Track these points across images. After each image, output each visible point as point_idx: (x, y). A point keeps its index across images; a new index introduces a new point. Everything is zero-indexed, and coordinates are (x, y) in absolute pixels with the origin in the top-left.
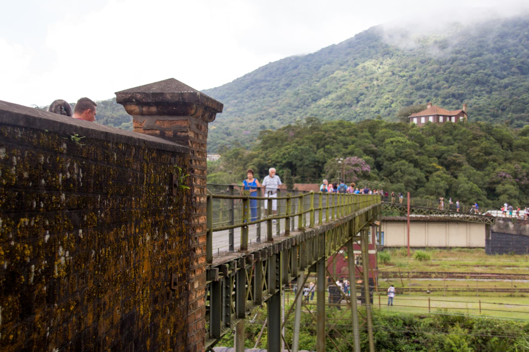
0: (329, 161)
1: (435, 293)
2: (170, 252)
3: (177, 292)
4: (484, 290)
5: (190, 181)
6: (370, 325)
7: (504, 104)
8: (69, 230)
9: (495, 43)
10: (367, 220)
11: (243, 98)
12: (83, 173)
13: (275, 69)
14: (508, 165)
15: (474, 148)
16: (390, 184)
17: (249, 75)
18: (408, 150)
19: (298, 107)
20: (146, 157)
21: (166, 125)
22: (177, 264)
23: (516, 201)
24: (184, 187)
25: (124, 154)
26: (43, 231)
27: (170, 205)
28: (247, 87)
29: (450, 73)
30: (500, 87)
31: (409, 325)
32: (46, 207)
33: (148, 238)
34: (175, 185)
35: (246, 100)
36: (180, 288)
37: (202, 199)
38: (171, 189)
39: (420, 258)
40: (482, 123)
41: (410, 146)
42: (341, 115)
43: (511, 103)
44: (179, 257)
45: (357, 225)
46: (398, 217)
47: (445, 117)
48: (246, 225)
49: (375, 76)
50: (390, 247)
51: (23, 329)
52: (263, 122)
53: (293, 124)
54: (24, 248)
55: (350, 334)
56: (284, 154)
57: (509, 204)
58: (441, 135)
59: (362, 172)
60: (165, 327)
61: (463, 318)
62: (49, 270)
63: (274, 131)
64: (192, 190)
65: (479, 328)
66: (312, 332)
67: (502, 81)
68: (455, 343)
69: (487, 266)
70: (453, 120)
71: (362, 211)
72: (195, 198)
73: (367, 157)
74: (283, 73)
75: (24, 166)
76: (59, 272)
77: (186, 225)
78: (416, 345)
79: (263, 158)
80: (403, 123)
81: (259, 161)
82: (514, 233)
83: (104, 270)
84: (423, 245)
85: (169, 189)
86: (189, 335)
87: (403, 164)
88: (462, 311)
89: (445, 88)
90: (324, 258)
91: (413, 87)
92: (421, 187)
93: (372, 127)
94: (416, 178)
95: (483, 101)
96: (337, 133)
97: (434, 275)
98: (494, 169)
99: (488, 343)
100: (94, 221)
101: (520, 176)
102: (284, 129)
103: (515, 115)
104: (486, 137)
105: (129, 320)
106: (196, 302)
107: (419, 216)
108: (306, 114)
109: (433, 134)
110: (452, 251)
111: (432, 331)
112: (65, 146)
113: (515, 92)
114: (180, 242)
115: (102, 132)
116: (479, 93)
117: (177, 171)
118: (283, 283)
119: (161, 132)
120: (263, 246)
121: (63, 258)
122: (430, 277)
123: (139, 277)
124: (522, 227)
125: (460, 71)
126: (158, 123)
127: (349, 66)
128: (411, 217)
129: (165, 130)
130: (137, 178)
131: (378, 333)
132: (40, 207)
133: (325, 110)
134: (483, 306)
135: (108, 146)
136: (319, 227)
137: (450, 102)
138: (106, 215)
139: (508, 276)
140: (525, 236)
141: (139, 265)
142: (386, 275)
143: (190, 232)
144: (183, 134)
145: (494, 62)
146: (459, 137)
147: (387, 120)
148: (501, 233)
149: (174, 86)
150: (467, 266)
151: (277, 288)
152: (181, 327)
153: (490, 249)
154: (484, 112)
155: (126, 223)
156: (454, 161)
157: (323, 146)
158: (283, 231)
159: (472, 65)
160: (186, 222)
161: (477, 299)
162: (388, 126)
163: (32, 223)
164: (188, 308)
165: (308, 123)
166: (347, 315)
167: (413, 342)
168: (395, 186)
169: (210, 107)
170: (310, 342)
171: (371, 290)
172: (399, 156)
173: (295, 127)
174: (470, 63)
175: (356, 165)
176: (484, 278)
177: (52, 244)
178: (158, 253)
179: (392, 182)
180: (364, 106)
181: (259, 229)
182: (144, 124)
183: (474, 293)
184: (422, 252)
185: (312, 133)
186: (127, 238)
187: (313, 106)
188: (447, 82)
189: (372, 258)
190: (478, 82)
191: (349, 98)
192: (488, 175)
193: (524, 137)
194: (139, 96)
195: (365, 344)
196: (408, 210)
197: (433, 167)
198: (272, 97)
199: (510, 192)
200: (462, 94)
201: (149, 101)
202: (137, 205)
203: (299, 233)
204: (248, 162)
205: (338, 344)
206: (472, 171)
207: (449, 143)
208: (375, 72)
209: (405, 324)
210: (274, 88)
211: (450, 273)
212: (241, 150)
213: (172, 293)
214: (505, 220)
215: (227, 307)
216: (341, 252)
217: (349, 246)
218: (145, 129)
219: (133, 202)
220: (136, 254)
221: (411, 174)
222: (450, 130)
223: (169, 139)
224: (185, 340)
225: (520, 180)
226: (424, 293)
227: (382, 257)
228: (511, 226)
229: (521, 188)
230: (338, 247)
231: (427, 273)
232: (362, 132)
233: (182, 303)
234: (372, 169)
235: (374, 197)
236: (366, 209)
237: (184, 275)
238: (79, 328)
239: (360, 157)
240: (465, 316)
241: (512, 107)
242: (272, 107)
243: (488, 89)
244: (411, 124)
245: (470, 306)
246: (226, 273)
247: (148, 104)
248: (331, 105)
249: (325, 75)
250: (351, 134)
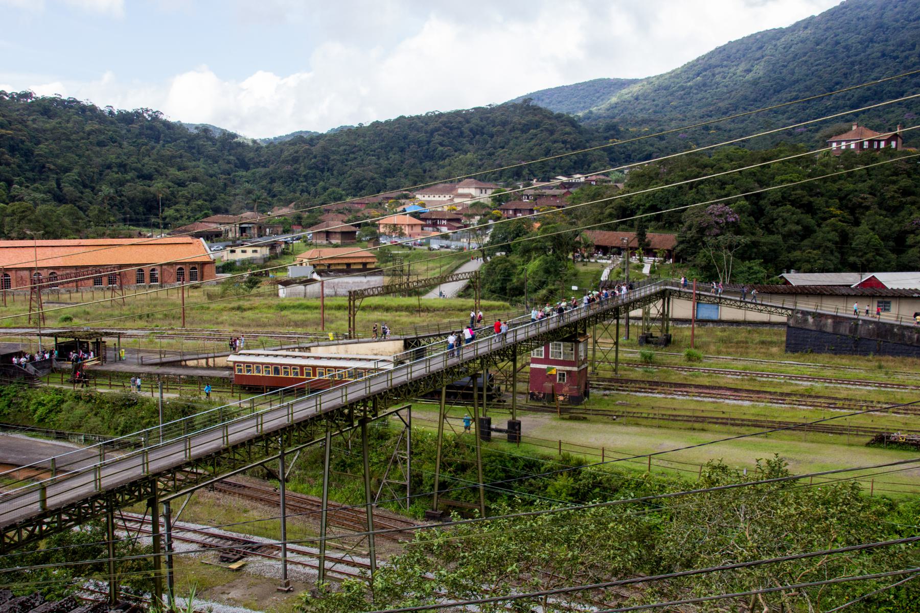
13: (734, 51)
82: (814, 328)
98: (911, 214)
140: (825, 332)
148: (798, 328)
180: (837, 99)
228: (810, 320)
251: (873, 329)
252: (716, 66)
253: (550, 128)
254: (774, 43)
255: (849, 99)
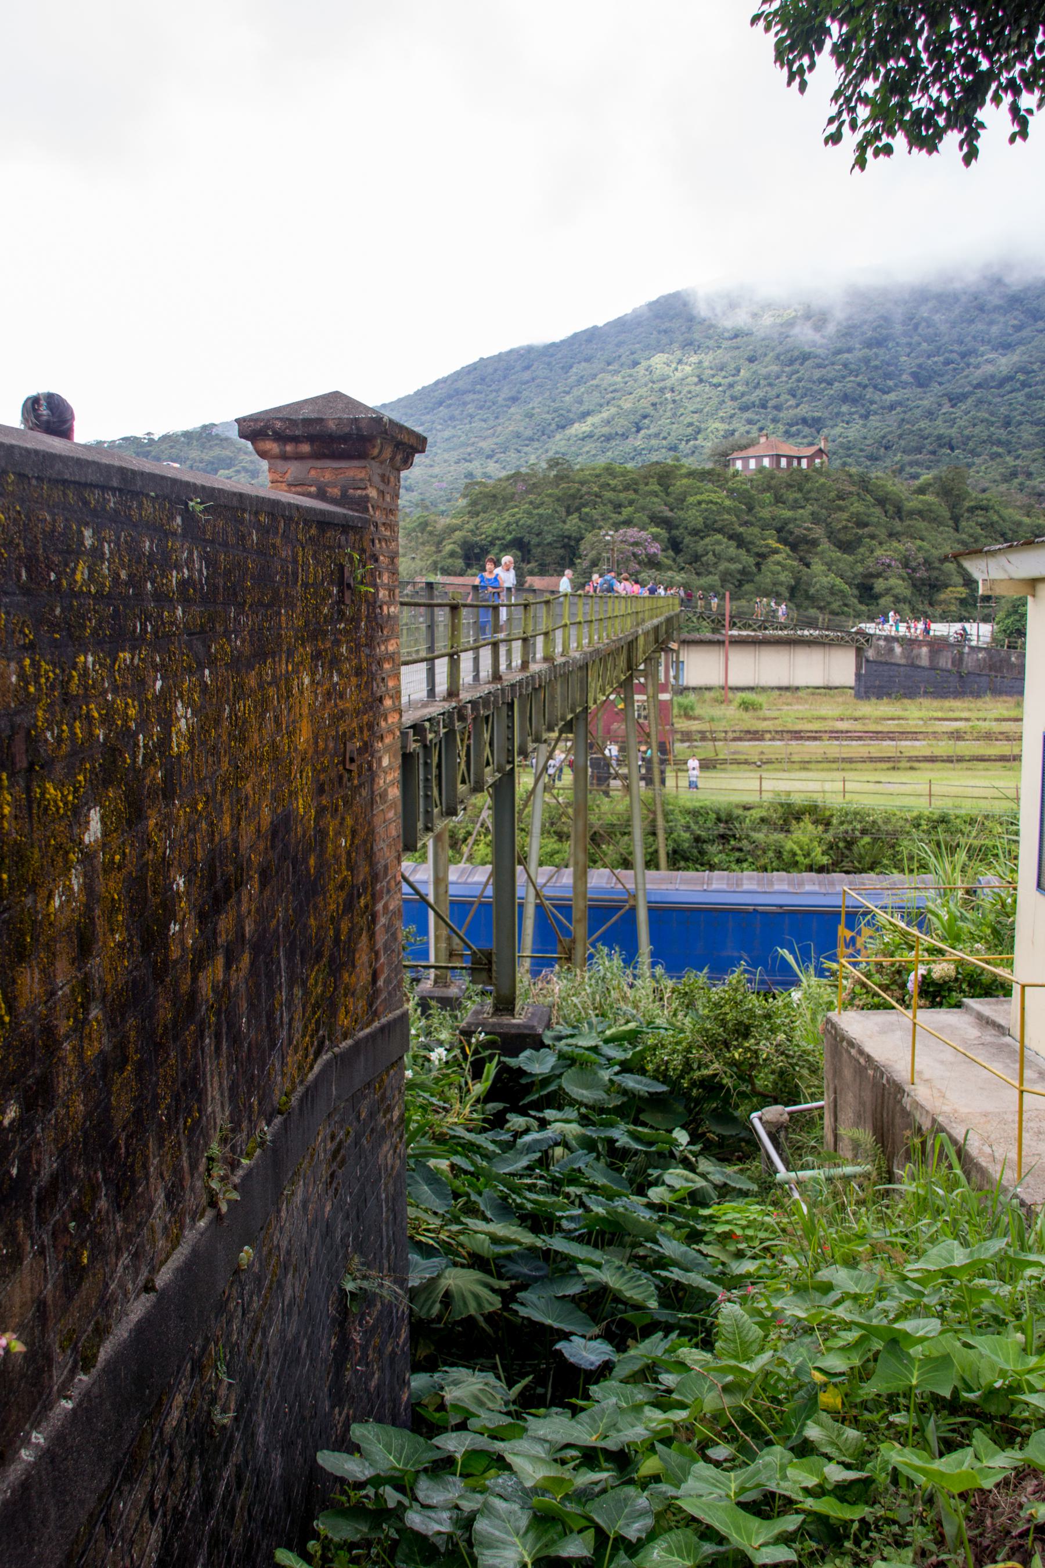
0: (589, 536)
1: (770, 766)
2: (342, 705)
3: (355, 774)
4: (850, 760)
5: (372, 577)
6: (660, 822)
7: (889, 437)
8: (190, 671)
9: (874, 329)
10: (656, 641)
11: (433, 422)
12: (207, 568)
13: (490, 370)
14: (895, 544)
15: (838, 515)
16: (695, 577)
17: (444, 380)
18: (726, 517)
19: (532, 439)
20: (300, 536)
21: (328, 477)
22: (354, 725)
23: (906, 607)
24: (363, 588)
25: (268, 532)
26: (152, 674)
27: (340, 621)
28: (440, 404)
29: (799, 380)
30: (883, 408)
31: (726, 822)
32: (155, 633)
33: (307, 681)
34: (349, 586)
35: (439, 427)
36: (360, 767)
37: (392, 609)
38: (341, 591)
39: (746, 706)
40: (853, 470)
41: (728, 510)
42: (609, 454)
43: (900, 437)
44: (358, 713)
45: (641, 650)
46: (708, 635)
47: (790, 458)
48: (456, 653)
49: (668, 383)
50: (694, 689)
51: (132, 845)
52: (470, 466)
53: (523, 470)
54: (127, 704)
55: (626, 838)
56: (508, 524)
57: (896, 612)
58: (783, 491)
59: (647, 555)
60: (338, 834)
61: (816, 807)
62: (165, 742)
63: (490, 482)
64: (375, 595)
65: (842, 823)
66: (561, 836)
67: (885, 397)
68: (802, 849)
69: (856, 719)
70: (804, 463)
71: (649, 625)
72: (381, 607)
73: (654, 530)
74: (505, 378)
75: (120, 559)
76: (178, 746)
77: (367, 656)
78: (737, 854)
79: (472, 531)
80: (718, 468)
81: (465, 537)
82: (903, 661)
83: (244, 740)
84: (751, 683)
85: (338, 592)
86: (375, 849)
87: (718, 543)
88: (815, 796)
89: (791, 406)
90: (587, 708)
91: (736, 404)
92: (748, 582)
93: (665, 476)
94: (740, 566)
95: (854, 432)
96: (601, 487)
97: (768, 736)
98: (872, 552)
99: (855, 848)
100: (226, 654)
101: (914, 564)
102: (508, 478)
103: (907, 458)
104: (858, 494)
105: (283, 824)
106: (386, 790)
107: (744, 633)
108: (547, 451)
109: (769, 488)
110: (800, 694)
111: (765, 831)
112: (179, 520)
113: (907, 416)
114: (358, 686)
115: (235, 494)
116: (846, 418)
117: (351, 558)
118: (519, 754)
119: (319, 489)
120: (486, 689)
121: (183, 721)
122: (761, 739)
123: (296, 749)
124: (915, 652)
125: (815, 378)
126: (313, 472)
127: (622, 365)
128: (732, 636)
129: (327, 485)
130: (287, 573)
131: (674, 835)
132: (146, 632)
133: (583, 444)
134: (849, 786)
135: (243, 518)
136: (577, 655)
137: (798, 433)
138: (243, 642)
139: (890, 736)
140: (919, 667)
141: (295, 728)
142: (687, 737)
143: (374, 668)
144: (359, 492)
145: (873, 363)
146: (813, 495)
147: (690, 463)
149: (340, 406)
150: (825, 719)
151: (509, 762)
152: (362, 834)
153: (862, 690)
154: (855, 451)
155: (273, 654)
156: (805, 536)
157: (578, 510)
158: (517, 662)
159: (837, 367)
160: (367, 651)
161: (839, 775)
162: (691, 474)
163: (136, 661)
164: (372, 802)
165: (551, 467)
166: (621, 807)
167: (732, 849)
168: (703, 581)
169: (403, 444)
170: (558, 852)
171: (663, 762)
172: (710, 527)
173: (527, 474)
174: (833, 364)
175: (636, 544)
176: (852, 739)
177: (165, 697)
178: (323, 704)
179: (698, 574)
180: (649, 437)
181: (476, 660)
182: (288, 475)
183: (835, 766)
184: (748, 696)
185: (557, 486)
186: (275, 682)
187: (558, 437)
188: (794, 396)
189: (664, 708)
190: (845, 398)
191: (622, 424)
192: (862, 561)
193: (921, 497)
194: (278, 425)
195: (652, 854)
196: (727, 623)
197: (767, 546)
198: (485, 421)
199: (897, 591)
200: (819, 419)
201: (297, 433)
202: (289, 622)
203: (545, 666)
204: (444, 539)
205: (606, 855)
206: (833, 555)
207: (795, 506)
208: (669, 377)
209: (719, 820)
210: (488, 404)
211: (796, 732)
212: (432, 517)
213: (346, 776)
214: (889, 639)
215: (427, 796)
216: (612, 697)
217: (627, 687)
218: (290, 485)
219: (283, 618)
220: (290, 710)
221: (731, 560)
222: (799, 481)
223: (333, 501)
224: (370, 857)
225: (914, 570)
226: (752, 767)
227: (680, 706)
228: (898, 649)
229: (914, 585)
230: (609, 690)
231: (756, 732)
232: (647, 484)
233: (364, 793)
234: (663, 550)
235: (667, 600)
236: (656, 621)
237: (365, 744)
238: (212, 841)
239: (643, 529)
240: (820, 804)
241: (903, 443)
242: (485, 438)
243: (863, 411)
244: (731, 470)
245: (828, 786)
246: (425, 738)
247: (295, 440)
248: (590, 436)
249: (581, 381)
250: (627, 488)
251: (984, 659)
252: (465, 392)
253: (251, 467)
254: (547, 359)
255: (665, 438)
